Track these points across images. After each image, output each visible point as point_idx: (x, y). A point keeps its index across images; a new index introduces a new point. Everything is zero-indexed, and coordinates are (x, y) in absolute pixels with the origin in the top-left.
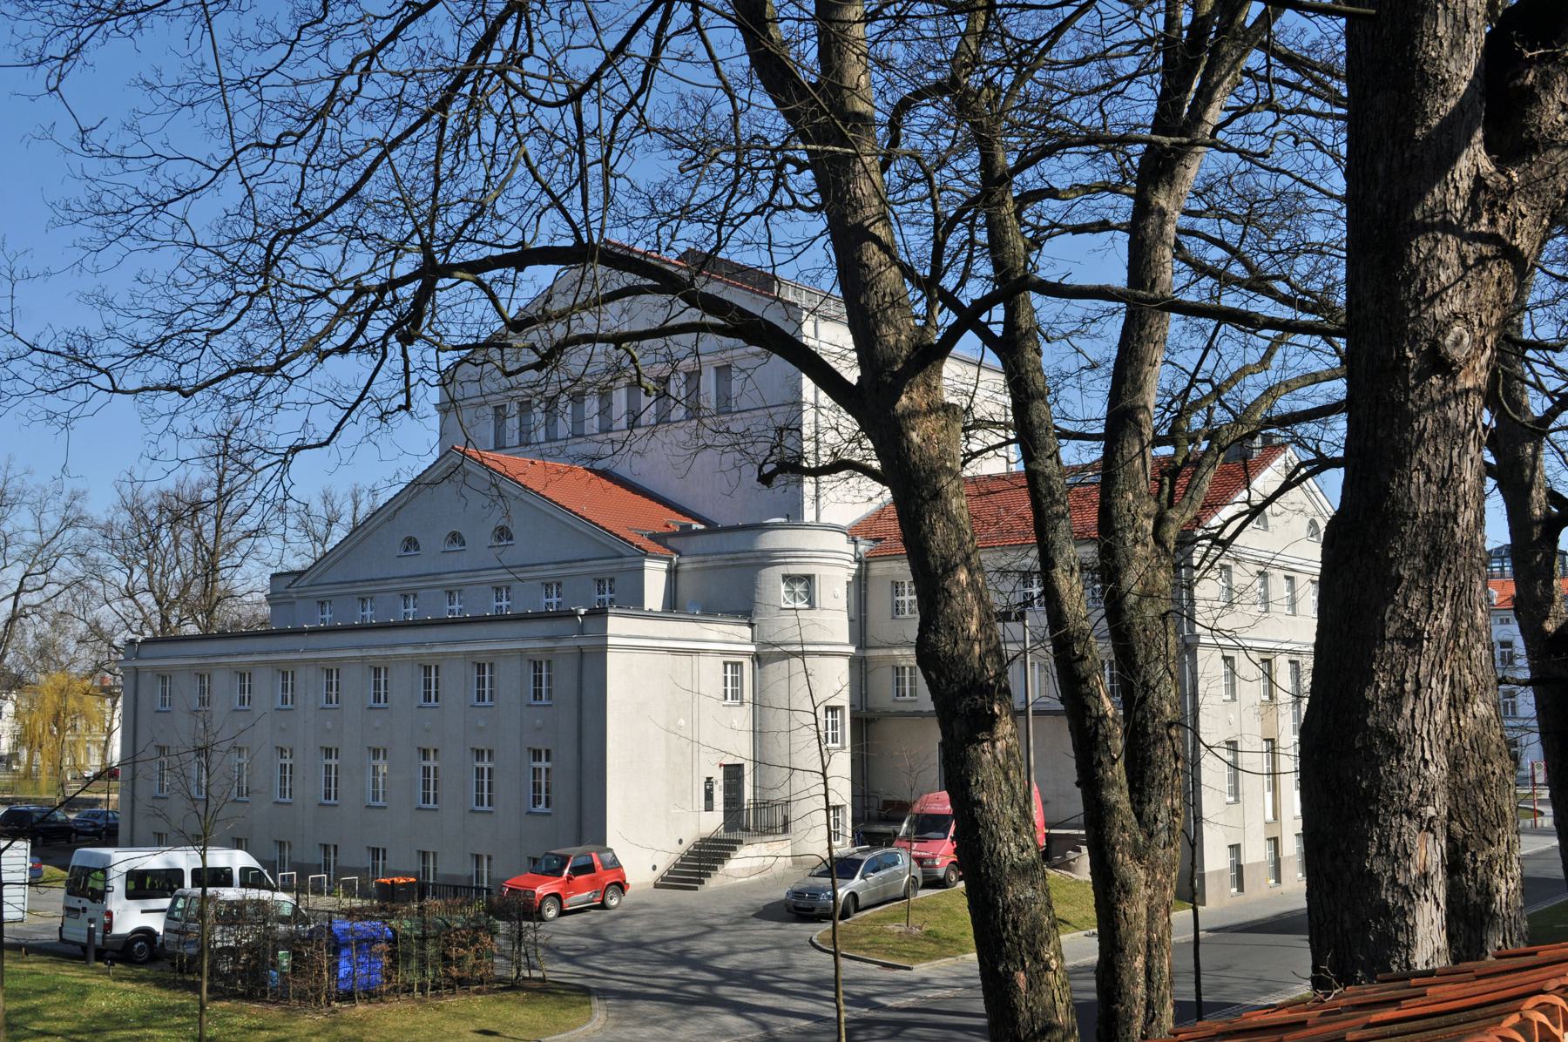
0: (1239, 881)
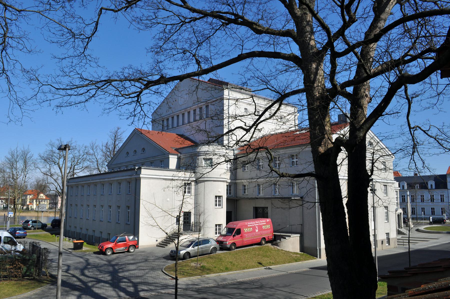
0: (389, 242)
